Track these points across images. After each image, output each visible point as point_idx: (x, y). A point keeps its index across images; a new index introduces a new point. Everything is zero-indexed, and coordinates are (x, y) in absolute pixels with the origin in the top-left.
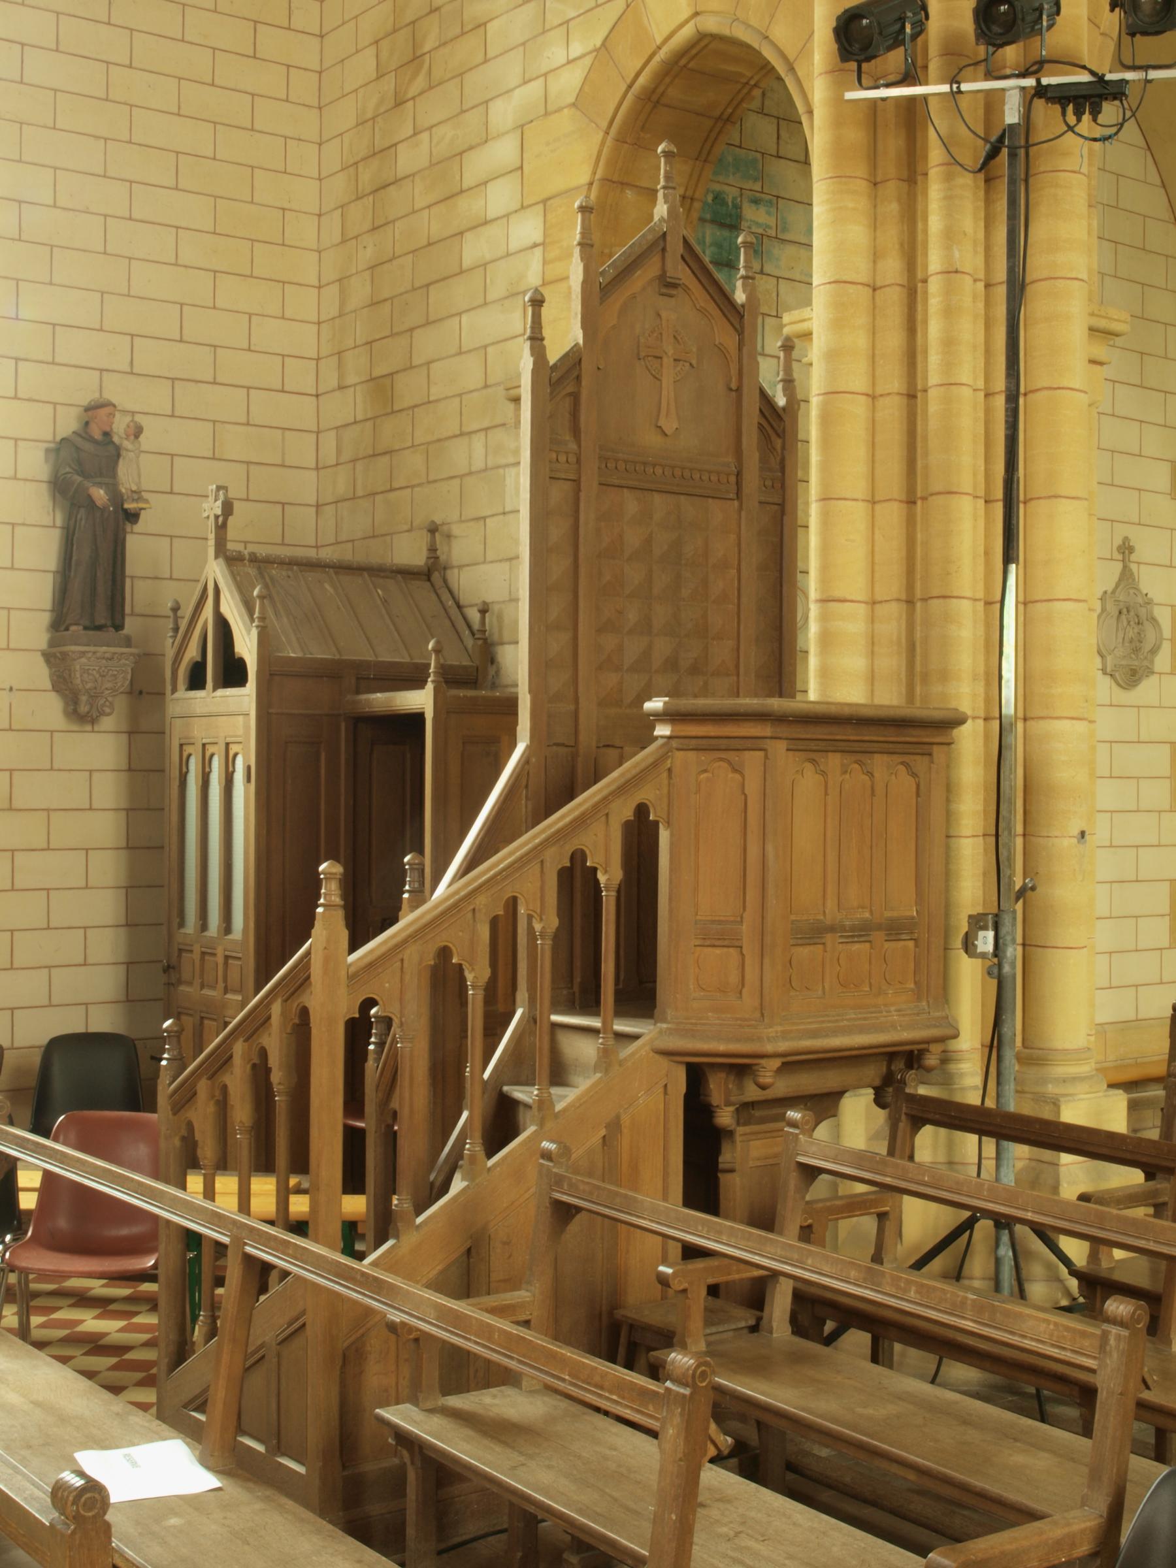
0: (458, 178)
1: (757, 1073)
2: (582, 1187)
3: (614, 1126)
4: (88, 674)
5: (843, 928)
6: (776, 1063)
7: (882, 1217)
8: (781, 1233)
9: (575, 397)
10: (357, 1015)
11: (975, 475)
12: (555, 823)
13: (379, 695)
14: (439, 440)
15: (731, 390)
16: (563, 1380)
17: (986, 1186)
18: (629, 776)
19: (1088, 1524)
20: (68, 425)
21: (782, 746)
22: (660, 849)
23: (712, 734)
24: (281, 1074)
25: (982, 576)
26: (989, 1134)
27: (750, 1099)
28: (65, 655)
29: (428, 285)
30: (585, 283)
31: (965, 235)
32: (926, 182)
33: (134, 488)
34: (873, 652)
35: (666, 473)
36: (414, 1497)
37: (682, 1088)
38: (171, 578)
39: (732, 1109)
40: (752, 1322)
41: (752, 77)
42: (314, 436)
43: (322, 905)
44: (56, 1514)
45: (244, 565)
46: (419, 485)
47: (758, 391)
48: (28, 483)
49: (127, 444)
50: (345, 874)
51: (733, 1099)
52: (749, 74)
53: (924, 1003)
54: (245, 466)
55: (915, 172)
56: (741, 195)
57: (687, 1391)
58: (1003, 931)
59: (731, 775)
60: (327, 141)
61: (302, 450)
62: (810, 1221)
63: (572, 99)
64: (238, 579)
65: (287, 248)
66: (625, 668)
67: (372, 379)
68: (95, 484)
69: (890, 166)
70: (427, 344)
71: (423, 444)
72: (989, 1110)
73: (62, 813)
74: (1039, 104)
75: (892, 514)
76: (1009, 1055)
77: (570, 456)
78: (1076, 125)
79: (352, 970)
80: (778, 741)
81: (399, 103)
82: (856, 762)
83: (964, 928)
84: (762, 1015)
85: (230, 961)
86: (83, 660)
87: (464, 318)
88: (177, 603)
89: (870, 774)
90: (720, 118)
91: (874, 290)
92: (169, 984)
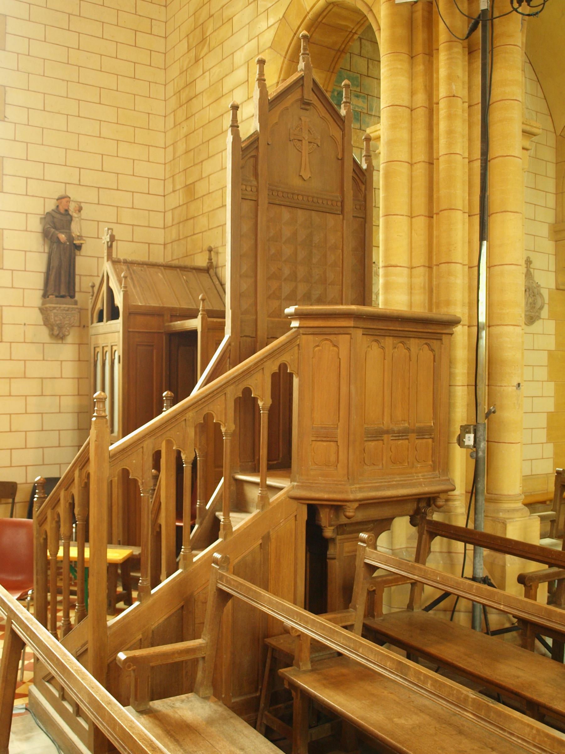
0: (221, 90)
1: (345, 510)
2: (232, 583)
3: (267, 538)
5: (393, 432)
6: (356, 505)
9: (256, 157)
11: (463, 201)
13: (179, 322)
14: (213, 210)
15: (338, 159)
17: (474, 587)
20: (51, 206)
21: (360, 332)
22: (294, 388)
23: (322, 325)
24: (79, 509)
25: (467, 253)
27: (343, 523)
31: (458, 77)
32: (438, 53)
33: (78, 234)
35: (304, 199)
37: (305, 517)
39: (332, 528)
41: (353, 29)
42: (163, 214)
47: (352, 160)
48: (32, 233)
49: (75, 215)
51: (333, 523)
52: (352, 27)
53: (437, 472)
58: (479, 434)
59: (332, 348)
60: (169, 83)
62: (374, 588)
63: (269, 45)
64: (117, 270)
65: (150, 131)
66: (283, 298)
68: (61, 232)
69: (419, 47)
70: (208, 167)
75: (421, 223)
76: (481, 499)
78: (518, 8)
80: (358, 329)
81: (197, 61)
82: (401, 342)
83: (458, 432)
84: (348, 478)
86: (55, 311)
89: (408, 349)
90: (339, 50)
91: (412, 111)
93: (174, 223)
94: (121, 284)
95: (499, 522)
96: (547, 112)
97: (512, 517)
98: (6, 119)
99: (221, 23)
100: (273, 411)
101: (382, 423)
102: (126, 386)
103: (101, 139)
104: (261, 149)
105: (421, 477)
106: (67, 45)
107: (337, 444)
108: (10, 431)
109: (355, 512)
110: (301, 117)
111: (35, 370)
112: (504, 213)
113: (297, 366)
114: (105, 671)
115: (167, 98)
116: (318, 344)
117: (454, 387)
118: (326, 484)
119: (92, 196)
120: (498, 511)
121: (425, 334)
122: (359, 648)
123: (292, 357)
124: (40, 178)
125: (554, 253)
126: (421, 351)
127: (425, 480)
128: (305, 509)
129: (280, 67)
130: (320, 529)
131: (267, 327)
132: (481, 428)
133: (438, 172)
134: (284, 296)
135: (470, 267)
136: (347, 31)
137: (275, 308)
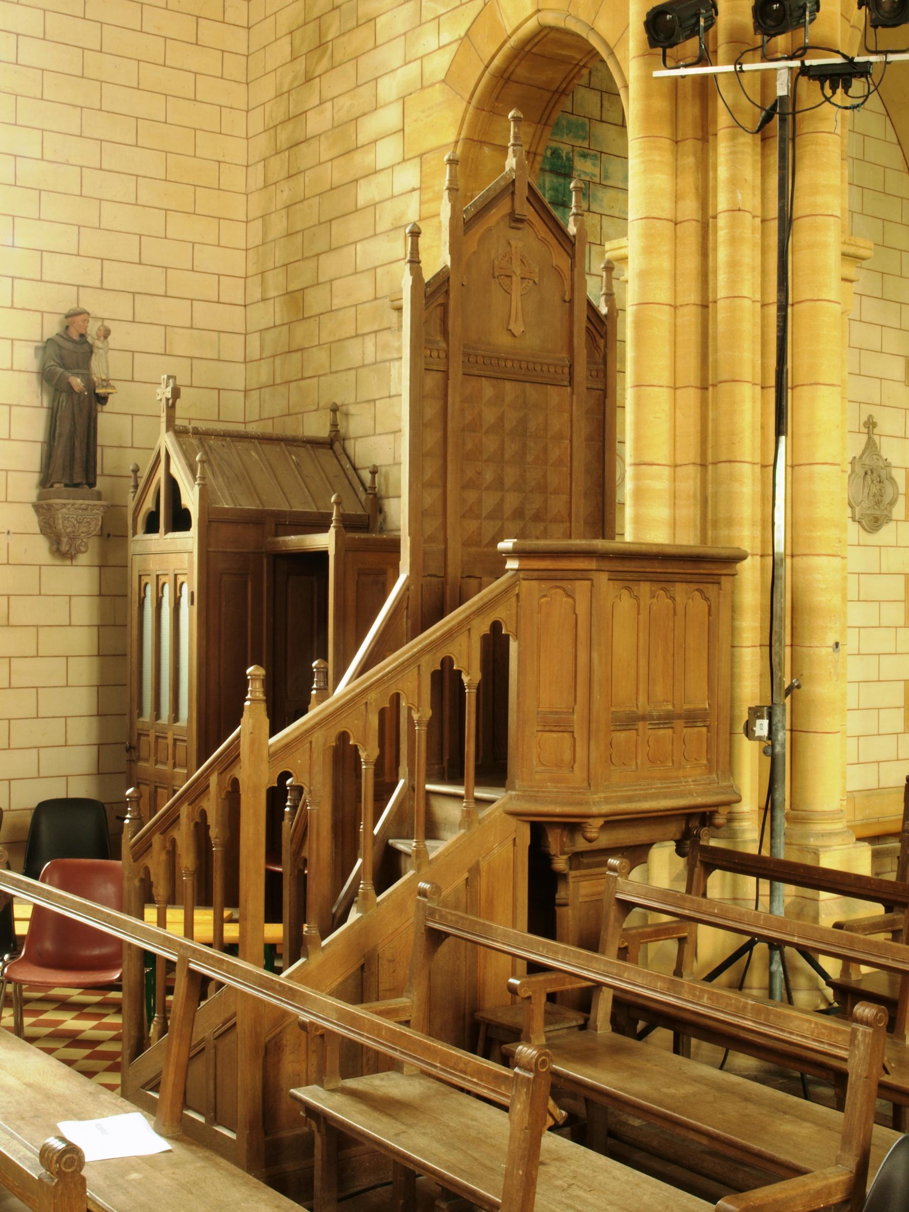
0: (354, 137)
3: (475, 870)
4: (68, 521)
5: (652, 718)
6: (600, 822)
7: (682, 941)
8: (603, 953)
9: (445, 307)
10: (276, 785)
11: (753, 367)
12: (429, 636)
13: (293, 537)
14: (340, 340)
15: (565, 301)
16: (436, 1067)
17: (762, 917)
18: (486, 600)
19: (841, 1178)
20: (53, 328)
21: (604, 576)
23: (551, 567)
26: (765, 877)
27: (579, 850)
28: (50, 506)
29: (331, 221)
33: (104, 377)
35: (515, 366)
36: (320, 1157)
37: (527, 841)
38: (132, 447)
39: (565, 857)
40: (581, 1022)
41: (581, 60)
42: (243, 337)
44: (43, 1171)
45: (189, 437)
46: (323, 375)
49: (98, 343)
51: (566, 849)
53: (714, 775)
54: (189, 360)
56: (573, 151)
57: (531, 1075)
58: (776, 719)
59: (565, 599)
60: (253, 109)
61: (234, 348)
62: (626, 944)
63: (442, 76)
64: (184, 447)
66: (484, 516)
68: (73, 374)
69: (688, 128)
70: (330, 265)
71: (327, 343)
72: (764, 859)
74: (803, 80)
75: (690, 397)
76: (780, 816)
79: (272, 750)
81: (308, 80)
83: (745, 717)
84: (589, 785)
86: (65, 510)
87: (359, 246)
88: (137, 466)
89: (673, 598)
91: (676, 224)
92: (130, 761)
95: (809, 851)
99: (354, 24)
100: (481, 689)
101: (635, 705)
102: (204, 643)
105: (692, 783)
106: (80, 45)
107: (573, 735)
109: (599, 833)
110: (510, 242)
112: (815, 387)
113: (515, 625)
114: (262, 1053)
115: (249, 136)
117: (740, 649)
118: (557, 792)
119: (120, 307)
120: (807, 836)
121: (696, 576)
122: (624, 972)
123: (508, 612)
127: (697, 787)
128: (526, 831)
129: (460, 118)
131: (462, 561)
132: (778, 711)
135: (764, 466)
136: (570, 63)
137: (473, 532)
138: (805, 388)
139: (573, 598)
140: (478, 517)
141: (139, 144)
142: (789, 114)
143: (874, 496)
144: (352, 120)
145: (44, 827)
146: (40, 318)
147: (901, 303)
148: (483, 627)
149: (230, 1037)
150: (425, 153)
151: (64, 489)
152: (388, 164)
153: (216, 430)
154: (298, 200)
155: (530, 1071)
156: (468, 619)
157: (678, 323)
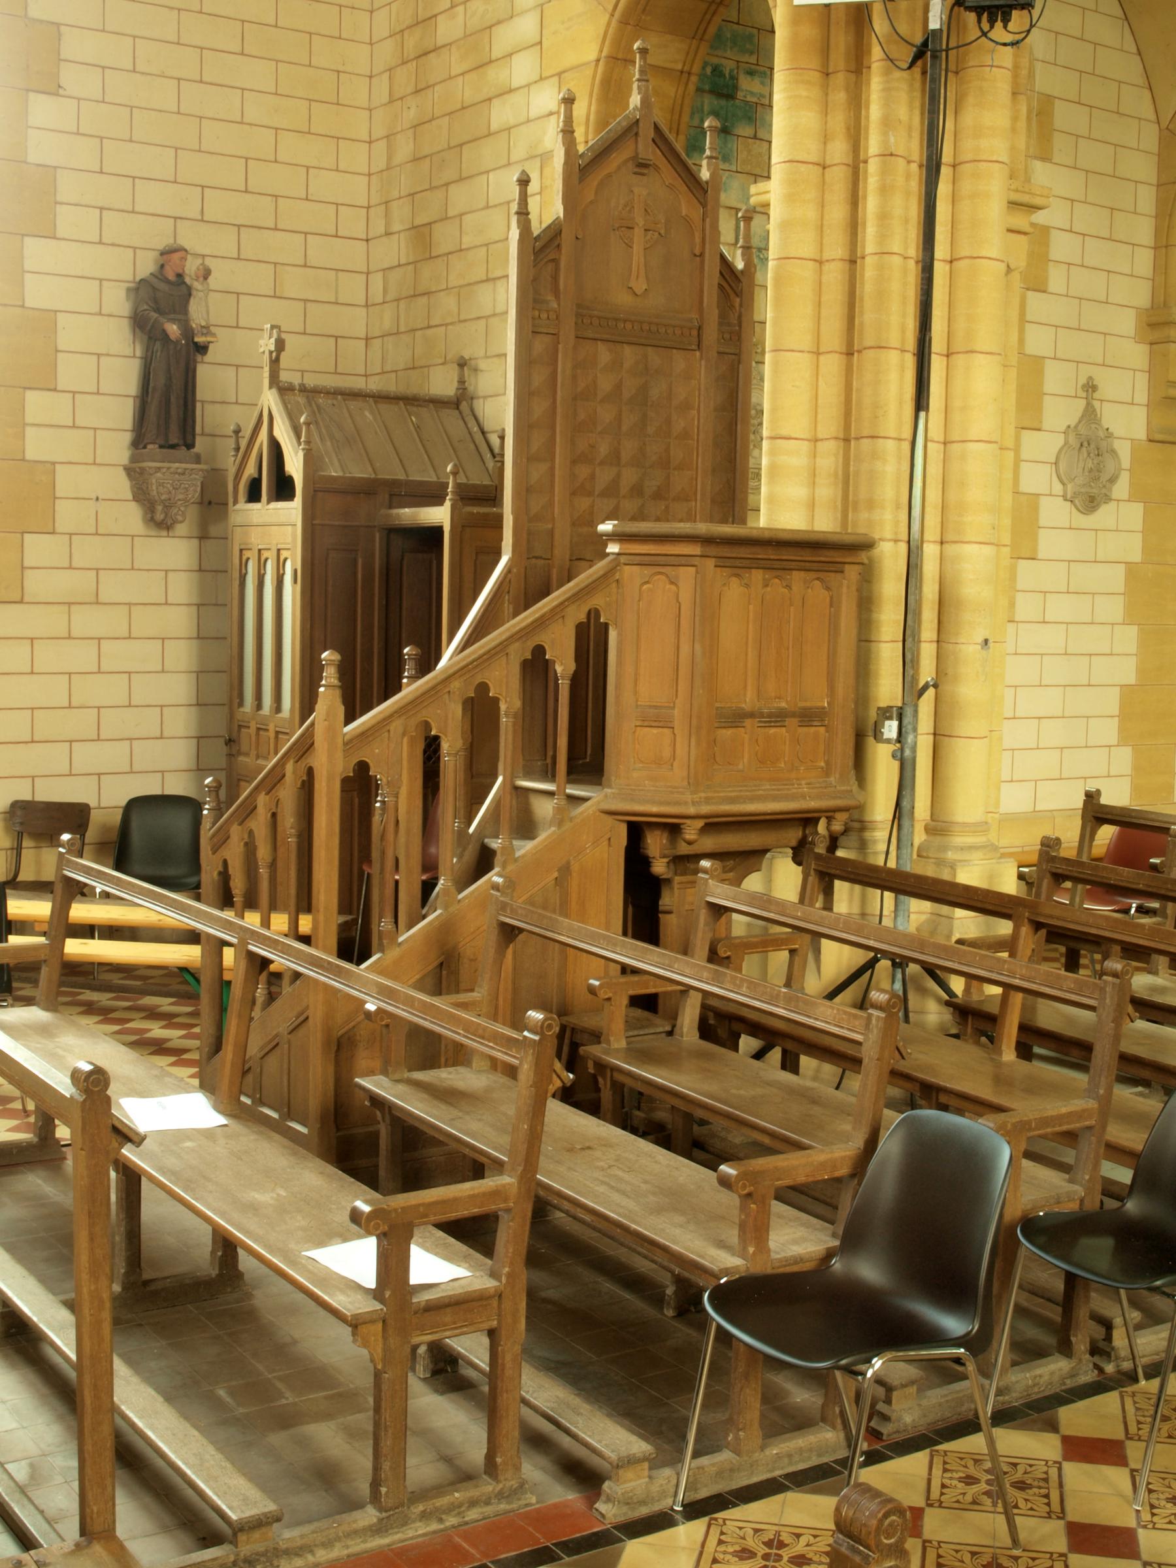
0: (487, 49)
4: (164, 487)
5: (762, 715)
6: (700, 823)
7: (792, 952)
8: (692, 957)
9: (555, 261)
10: (352, 774)
11: (903, 331)
12: (519, 623)
13: (407, 510)
14: (470, 284)
15: (695, 255)
16: (459, 1034)
18: (583, 585)
19: (848, 1153)
20: (146, 266)
23: (653, 552)
26: (890, 889)
28: (143, 470)
29: (461, 145)
30: (566, 163)
33: (203, 324)
34: (814, 483)
36: (385, 1148)
37: (624, 842)
38: (237, 403)
39: (666, 860)
40: (668, 1028)
43: (323, 686)
44: (73, 1090)
45: (294, 395)
46: (451, 324)
47: (719, 256)
49: (197, 285)
50: (342, 662)
54: (302, 304)
55: (862, 64)
56: (738, 68)
57: (537, 1038)
58: (905, 721)
59: (668, 586)
61: (353, 289)
62: (729, 953)
66: (596, 493)
67: (414, 227)
70: (459, 197)
71: (455, 287)
72: (890, 871)
73: (142, 607)
75: (832, 365)
77: (551, 313)
79: (347, 737)
84: (689, 783)
85: (280, 736)
86: (159, 475)
87: (491, 175)
88: (239, 426)
91: (824, 168)
92: (230, 755)
93: (388, 298)
94: (298, 437)
96: (1141, 81)
97: (967, 858)
98: (61, 92)
100: (576, 681)
103: (244, 126)
104: (564, 250)
108: (70, 707)
111: (113, 588)
116: (646, 580)
119: (224, 242)
120: (944, 848)
121: (816, 564)
124: (126, 208)
125: (1147, 369)
126: (810, 590)
128: (623, 829)
130: (646, 862)
133: (862, 283)
134: (597, 491)
138: (960, 356)
139: (676, 585)
140: (590, 494)
141: (245, 52)
142: (942, 50)
143: (1090, 472)
144: (486, 28)
145: (135, 824)
146: (132, 255)
147: (1134, 245)
148: (578, 614)
149: (302, 1032)
150: (564, 72)
151: (158, 450)
152: (524, 83)
153: (325, 387)
154: (426, 119)
155: (535, 1033)
156: (562, 606)
157: (824, 281)
